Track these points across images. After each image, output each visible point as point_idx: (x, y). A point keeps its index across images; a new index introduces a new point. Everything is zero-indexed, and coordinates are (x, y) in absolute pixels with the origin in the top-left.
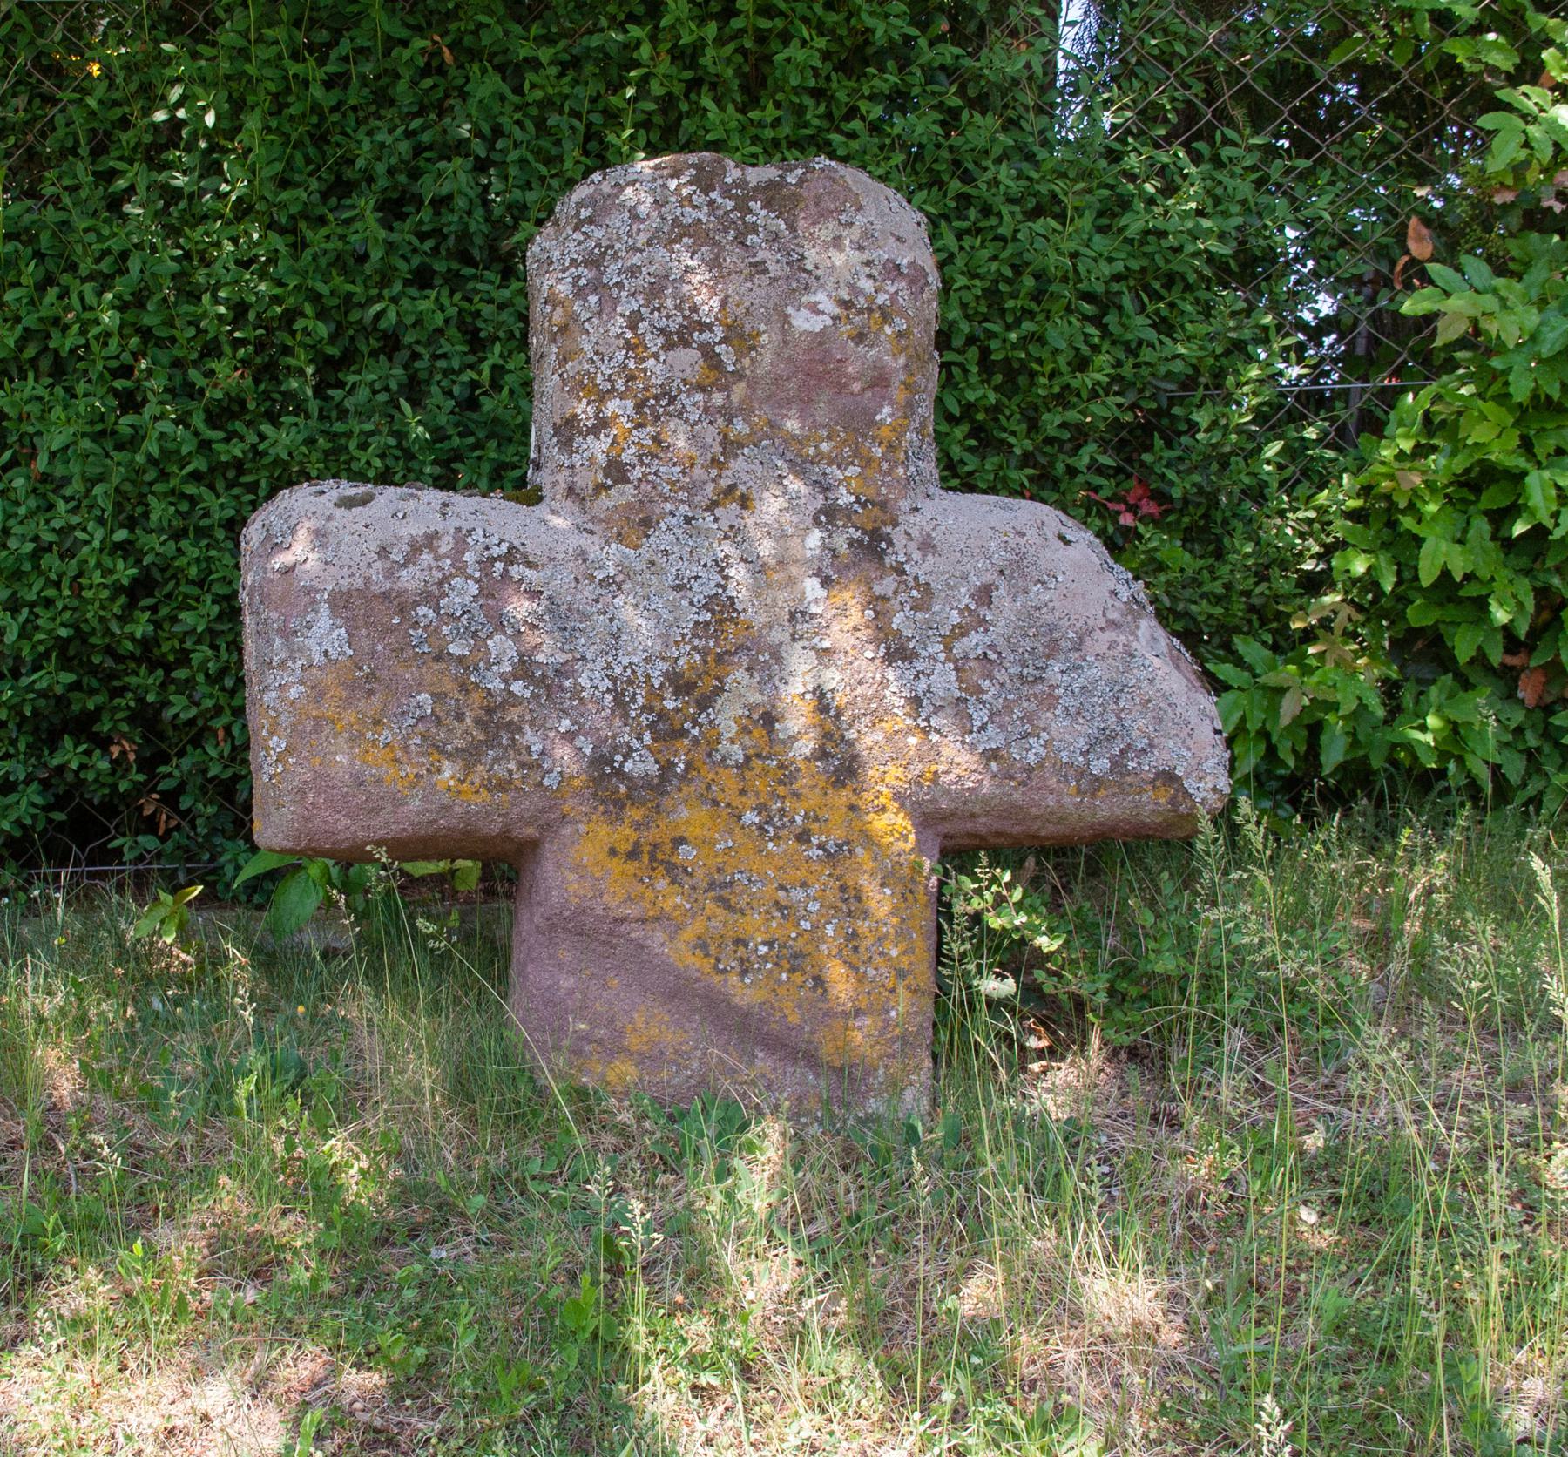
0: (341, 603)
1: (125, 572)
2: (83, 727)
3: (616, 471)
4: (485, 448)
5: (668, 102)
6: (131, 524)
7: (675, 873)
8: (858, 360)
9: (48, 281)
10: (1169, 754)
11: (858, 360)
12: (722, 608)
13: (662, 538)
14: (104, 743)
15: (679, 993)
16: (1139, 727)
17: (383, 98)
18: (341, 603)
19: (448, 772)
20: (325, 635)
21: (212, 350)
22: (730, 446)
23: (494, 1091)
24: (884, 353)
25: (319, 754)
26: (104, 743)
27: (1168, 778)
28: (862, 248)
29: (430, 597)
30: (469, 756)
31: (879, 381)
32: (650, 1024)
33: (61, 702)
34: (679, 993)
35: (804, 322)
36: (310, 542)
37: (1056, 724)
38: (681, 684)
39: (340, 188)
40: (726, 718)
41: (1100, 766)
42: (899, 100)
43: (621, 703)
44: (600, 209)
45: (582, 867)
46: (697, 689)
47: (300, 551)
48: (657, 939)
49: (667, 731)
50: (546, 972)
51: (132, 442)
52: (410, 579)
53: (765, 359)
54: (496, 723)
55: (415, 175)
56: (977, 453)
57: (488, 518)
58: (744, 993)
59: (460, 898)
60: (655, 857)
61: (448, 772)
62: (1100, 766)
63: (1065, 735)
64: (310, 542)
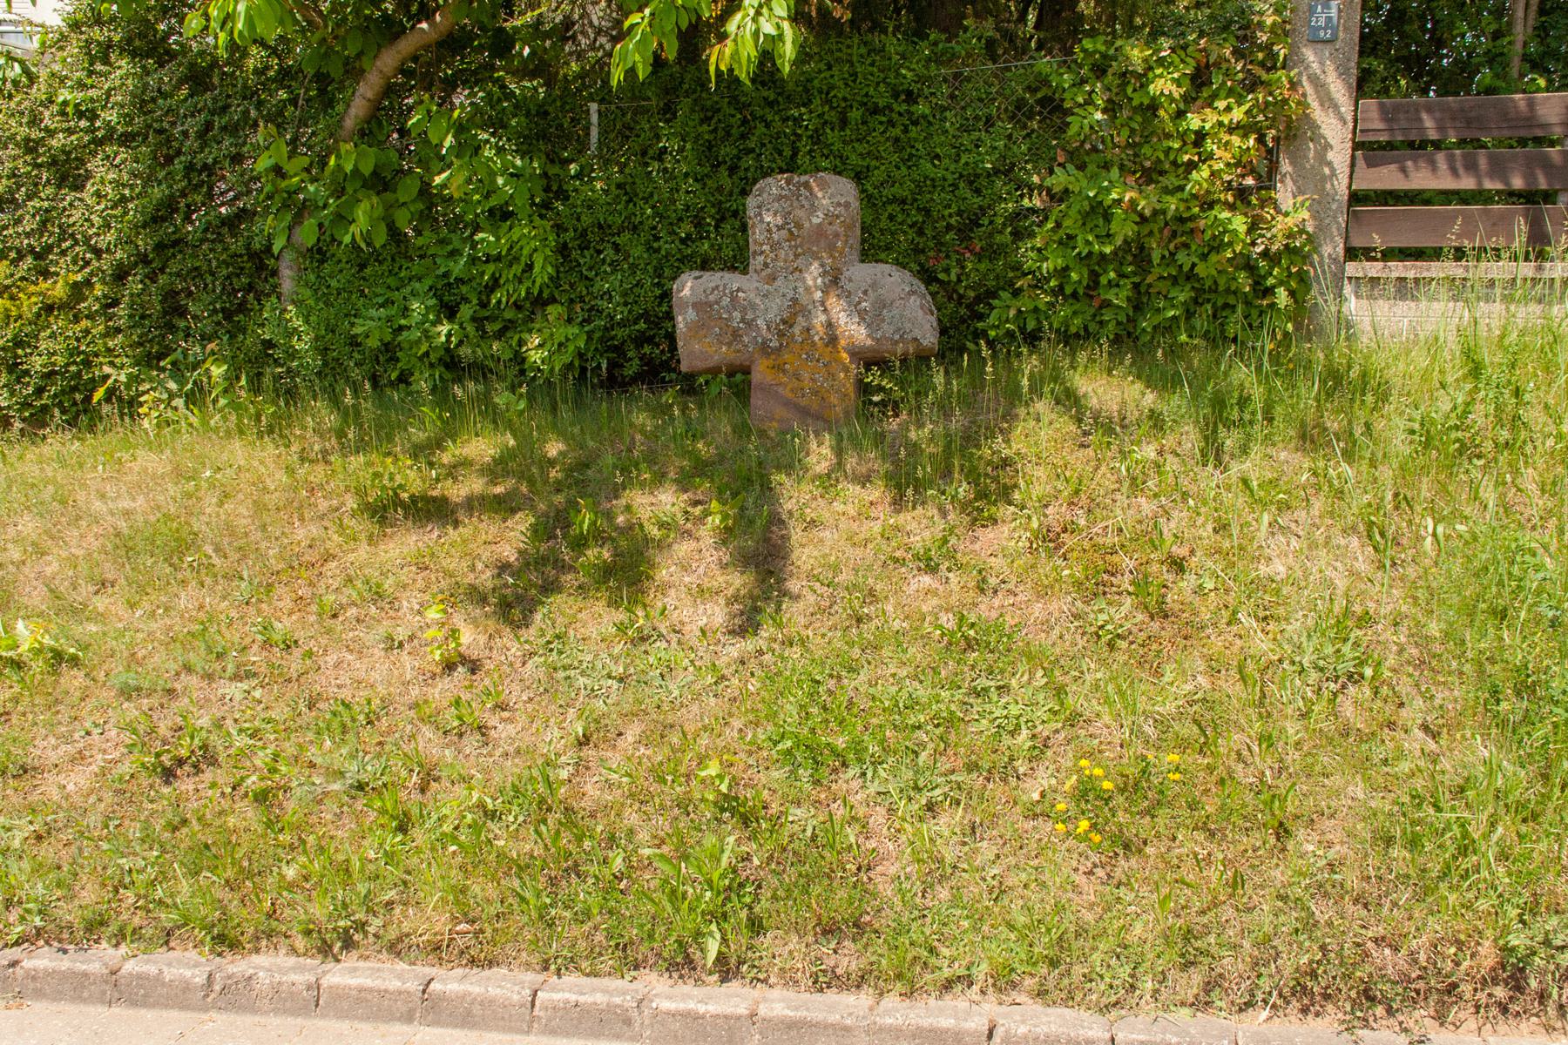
0: (694, 305)
1: (658, 292)
2: (650, 340)
3: (766, 265)
4: (738, 262)
5: (816, 131)
6: (659, 276)
7: (784, 371)
8: (830, 230)
9: (631, 200)
10: (917, 333)
11: (830, 230)
12: (795, 301)
13: (778, 283)
14: (658, 346)
15: (787, 403)
16: (908, 326)
17: (728, 134)
18: (694, 305)
19: (724, 349)
20: (691, 314)
21: (680, 219)
22: (797, 256)
23: (742, 431)
24: (836, 227)
25: (697, 348)
26: (658, 346)
27: (916, 339)
28: (832, 198)
29: (717, 303)
30: (729, 344)
31: (837, 235)
32: (780, 412)
33: (643, 333)
34: (787, 403)
35: (815, 221)
36: (687, 287)
37: (885, 326)
38: (784, 322)
39: (716, 167)
40: (797, 330)
41: (897, 337)
42: (891, 123)
43: (769, 328)
44: (761, 191)
45: (761, 372)
46: (788, 323)
47: (686, 292)
48: (780, 390)
49: (781, 334)
50: (757, 400)
51: (658, 251)
52: (712, 298)
53: (804, 232)
54: (736, 334)
55: (739, 159)
56: (868, 253)
57: (734, 280)
58: (803, 402)
59: (738, 379)
60: (779, 368)
61: (724, 349)
62: (897, 337)
63: (887, 329)
64: (687, 287)
